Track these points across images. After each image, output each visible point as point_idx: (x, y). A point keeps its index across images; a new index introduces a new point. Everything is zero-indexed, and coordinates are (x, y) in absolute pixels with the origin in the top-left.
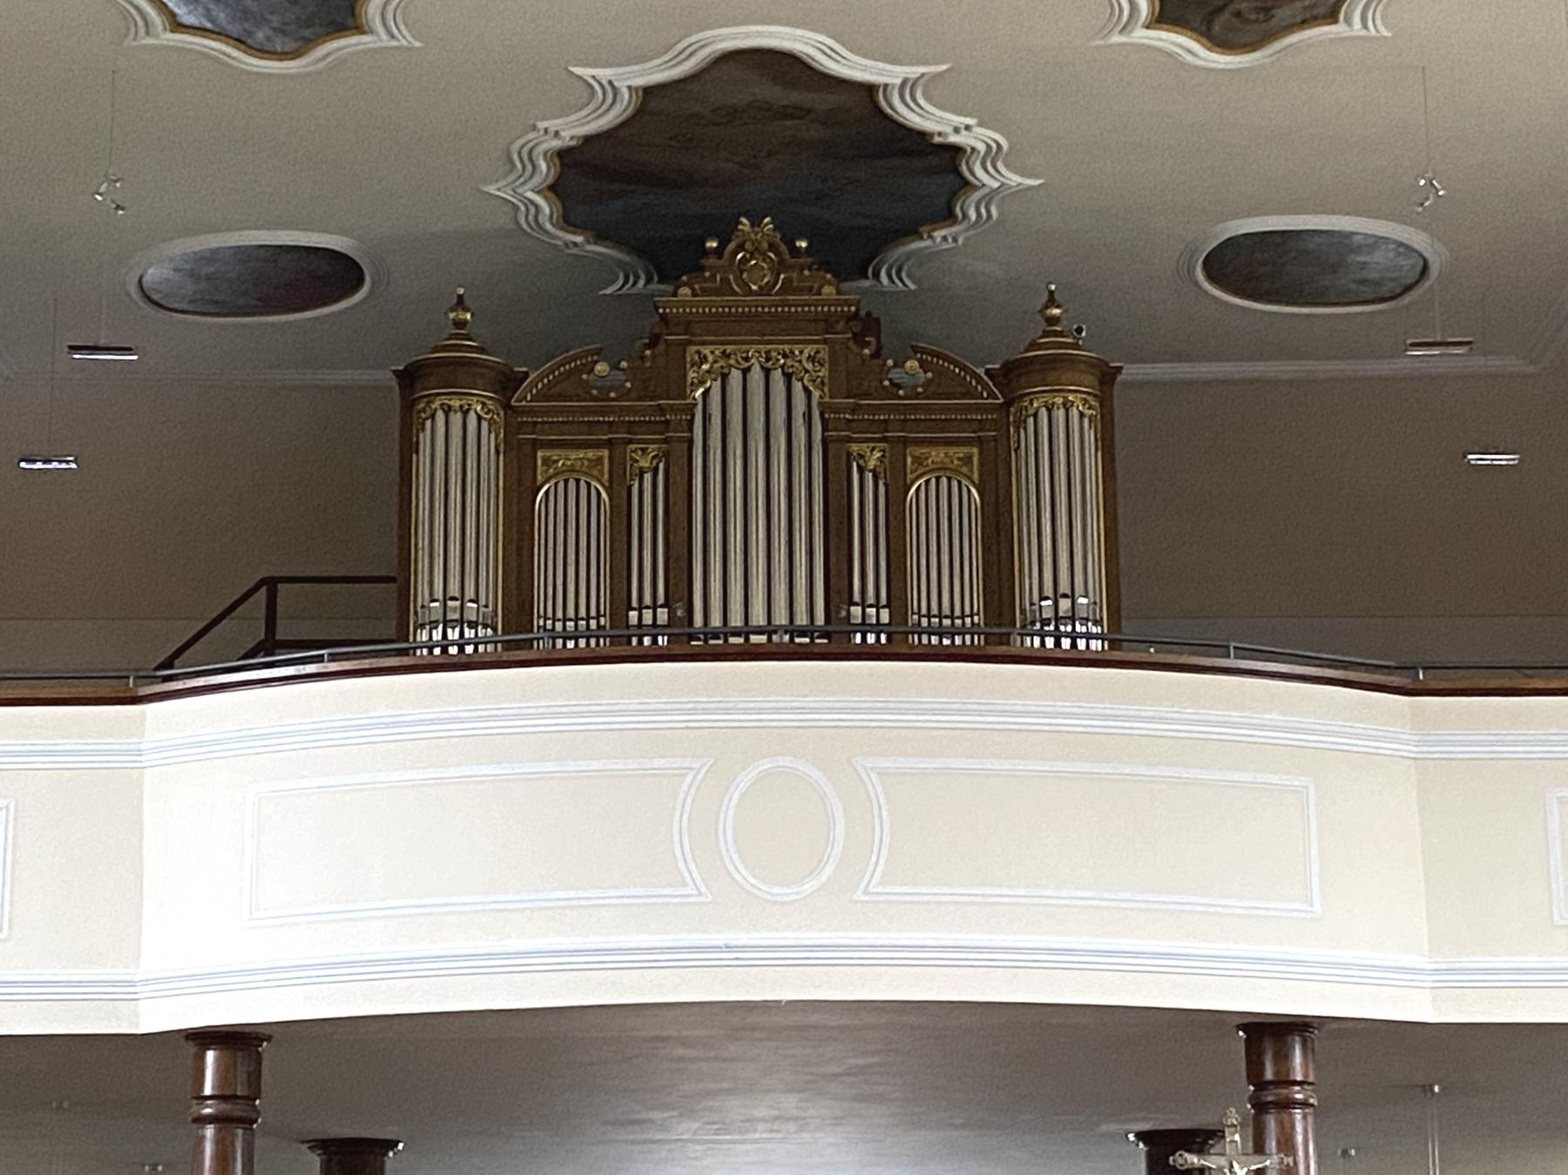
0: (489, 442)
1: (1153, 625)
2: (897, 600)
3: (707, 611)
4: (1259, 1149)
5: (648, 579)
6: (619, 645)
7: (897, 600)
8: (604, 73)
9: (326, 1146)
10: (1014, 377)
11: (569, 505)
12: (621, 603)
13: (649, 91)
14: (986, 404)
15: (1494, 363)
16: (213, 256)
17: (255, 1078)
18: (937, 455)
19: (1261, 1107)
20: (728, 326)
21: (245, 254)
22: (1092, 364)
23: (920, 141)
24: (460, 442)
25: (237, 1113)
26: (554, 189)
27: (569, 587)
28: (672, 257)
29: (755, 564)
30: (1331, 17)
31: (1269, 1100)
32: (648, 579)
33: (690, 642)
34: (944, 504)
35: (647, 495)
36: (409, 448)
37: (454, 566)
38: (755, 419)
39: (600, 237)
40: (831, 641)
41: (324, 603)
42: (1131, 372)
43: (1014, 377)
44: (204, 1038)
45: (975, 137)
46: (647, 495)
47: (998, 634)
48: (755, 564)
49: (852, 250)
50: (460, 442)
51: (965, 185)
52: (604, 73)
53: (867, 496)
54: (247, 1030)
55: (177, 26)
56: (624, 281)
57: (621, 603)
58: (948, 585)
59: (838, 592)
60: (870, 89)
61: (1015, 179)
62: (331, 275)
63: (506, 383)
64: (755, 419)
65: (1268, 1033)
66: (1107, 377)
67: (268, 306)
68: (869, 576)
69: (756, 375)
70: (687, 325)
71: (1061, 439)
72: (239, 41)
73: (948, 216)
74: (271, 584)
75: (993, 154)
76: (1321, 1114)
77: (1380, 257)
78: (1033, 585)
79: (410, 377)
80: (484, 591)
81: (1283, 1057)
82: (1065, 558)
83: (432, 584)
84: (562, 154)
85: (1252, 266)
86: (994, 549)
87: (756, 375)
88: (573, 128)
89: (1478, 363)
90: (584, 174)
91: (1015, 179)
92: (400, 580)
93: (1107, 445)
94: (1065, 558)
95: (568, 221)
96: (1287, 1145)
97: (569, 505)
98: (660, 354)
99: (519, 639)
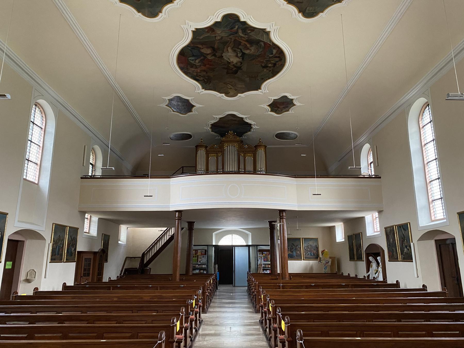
0: (204, 153)
1: (270, 171)
2: (245, 169)
3: (226, 170)
4: (280, 222)
5: (220, 167)
6: (217, 173)
7: (245, 169)
8: (216, 116)
9: (188, 222)
10: (256, 147)
11: (212, 159)
12: (217, 169)
13: (220, 118)
14: (253, 150)
15: (304, 146)
16: (176, 135)
17: (181, 215)
18: (249, 154)
19: (280, 218)
20: (227, 142)
21: (180, 134)
22: (264, 146)
23: (247, 123)
24: (202, 153)
25: (180, 219)
26: (211, 128)
27: (212, 167)
28: (223, 135)
29: (231, 165)
30: (288, 111)
31: (281, 218)
32: (220, 167)
33: (224, 173)
34: (249, 159)
35: (220, 158)
36: (196, 154)
37: (201, 166)
38: (231, 151)
39: (215, 133)
40: (238, 173)
41: (188, 168)
42: (268, 146)
43: (256, 147)
44: (176, 211)
45: (253, 123)
46: (220, 158)
47: (255, 172)
48: (231, 165)
49: (240, 134)
50: (202, 153)
51: (252, 128)
52: (216, 116)
53: (242, 158)
54: (286, 265)
55: (174, 111)
56: (218, 137)
57: (217, 169)
58: (250, 167)
59: (239, 168)
60: (242, 118)
61: (257, 127)
62: (189, 136)
63: (206, 147)
64: (231, 151)
65: (281, 211)
66: (266, 147)
67: (183, 139)
68: (242, 166)
69: (231, 147)
70: (224, 141)
71: (261, 153)
72: (180, 113)
73: (250, 131)
74: (183, 167)
75: (254, 125)
76: (286, 219)
77: (293, 135)
78: (258, 168)
79: (197, 147)
80: (204, 168)
81: (283, 214)
82: (261, 165)
83: (199, 167)
84: (212, 124)
85: (280, 136)
86: (391, 236)
87: (231, 147)
88: (213, 122)
89: (302, 146)
90: (214, 126)
91: (257, 127)
92: (196, 167)
93: (265, 153)
94: (261, 165)
95: (212, 131)
96: (283, 222)
97: (212, 159)
98: (221, 145)
99: (207, 172)
